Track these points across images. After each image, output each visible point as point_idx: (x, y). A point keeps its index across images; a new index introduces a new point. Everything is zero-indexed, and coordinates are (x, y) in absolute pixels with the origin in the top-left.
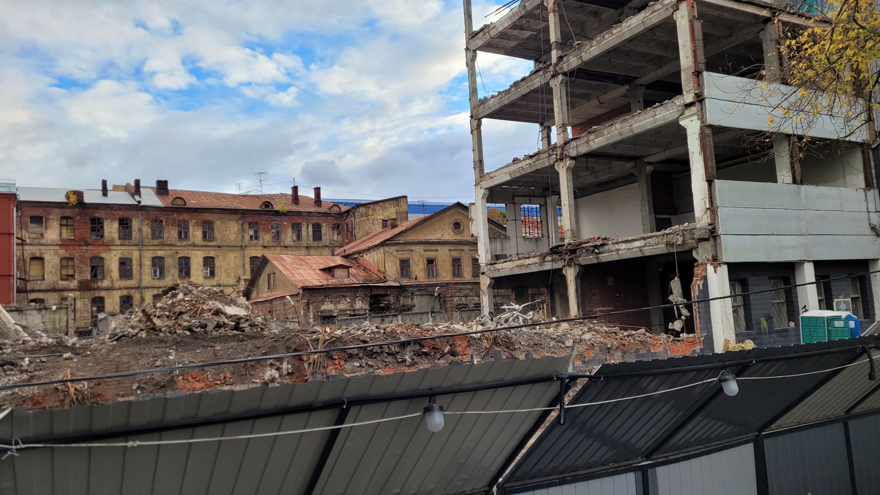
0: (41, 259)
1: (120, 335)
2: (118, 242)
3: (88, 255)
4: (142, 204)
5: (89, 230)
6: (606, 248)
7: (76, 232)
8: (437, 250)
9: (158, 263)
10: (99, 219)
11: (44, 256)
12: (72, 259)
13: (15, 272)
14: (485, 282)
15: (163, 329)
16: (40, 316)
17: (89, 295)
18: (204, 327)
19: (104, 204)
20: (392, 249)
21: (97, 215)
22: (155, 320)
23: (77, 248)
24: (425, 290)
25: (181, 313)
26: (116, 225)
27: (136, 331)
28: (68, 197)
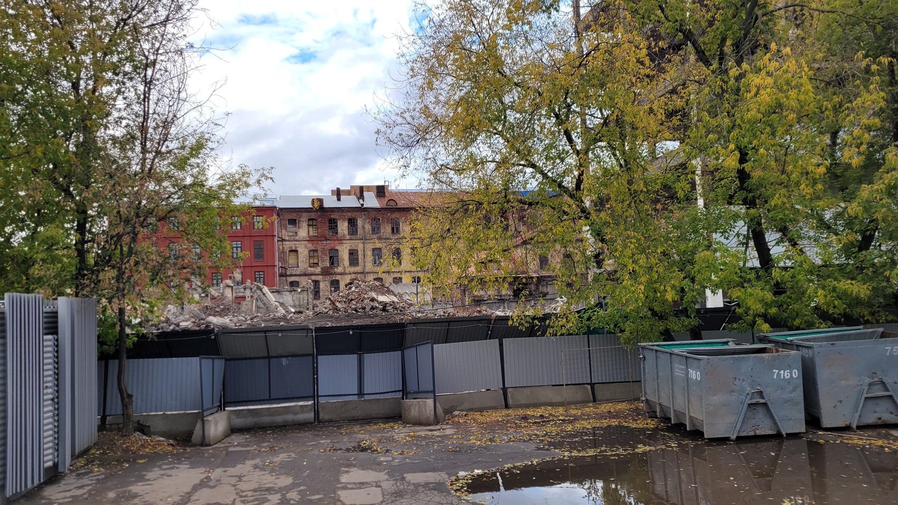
0: (296, 251)
2: (348, 237)
9: (377, 252)
12: (316, 251)
13: (277, 263)
17: (328, 278)
18: (364, 308)
21: (332, 217)
22: (337, 304)
25: (352, 300)
26: (346, 224)
28: (313, 204)
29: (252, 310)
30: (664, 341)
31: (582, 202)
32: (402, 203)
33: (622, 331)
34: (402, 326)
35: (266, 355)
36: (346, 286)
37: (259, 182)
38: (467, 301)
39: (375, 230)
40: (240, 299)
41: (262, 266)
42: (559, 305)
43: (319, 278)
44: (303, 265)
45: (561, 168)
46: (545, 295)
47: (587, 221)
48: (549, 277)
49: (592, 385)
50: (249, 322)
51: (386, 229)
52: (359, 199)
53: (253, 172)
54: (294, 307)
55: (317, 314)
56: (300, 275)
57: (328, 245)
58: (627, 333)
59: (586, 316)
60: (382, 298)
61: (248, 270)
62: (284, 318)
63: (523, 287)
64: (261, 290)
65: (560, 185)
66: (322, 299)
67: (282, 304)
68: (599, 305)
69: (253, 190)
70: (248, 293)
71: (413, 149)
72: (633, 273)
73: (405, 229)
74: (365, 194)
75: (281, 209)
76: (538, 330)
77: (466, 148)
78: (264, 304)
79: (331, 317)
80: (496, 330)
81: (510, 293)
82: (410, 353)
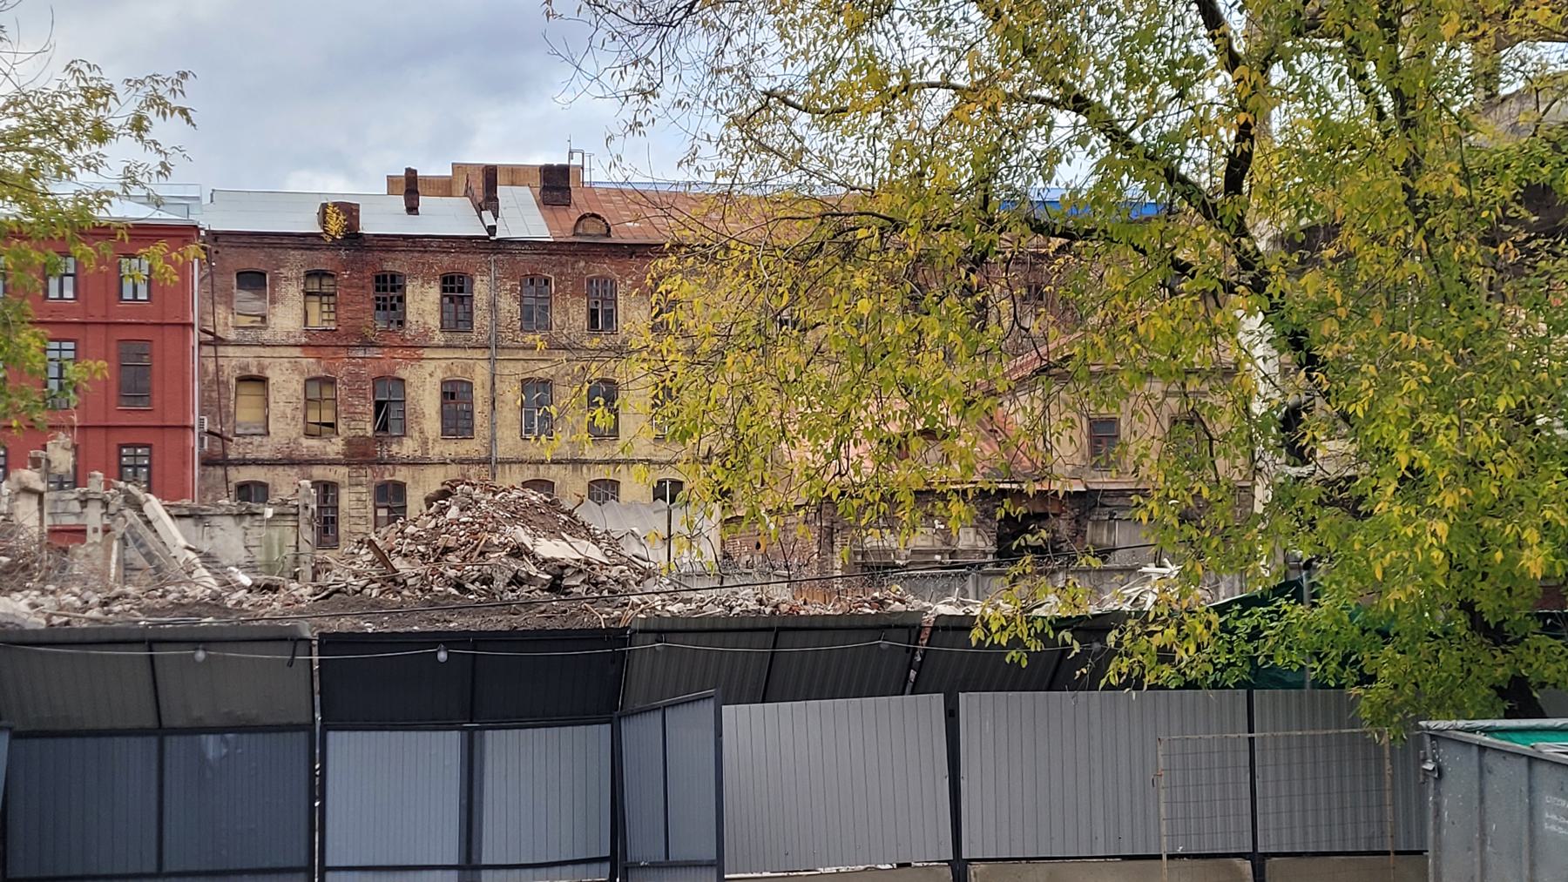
0: (262, 380)
1: (331, 588)
2: (439, 338)
3: (370, 371)
4: (499, 235)
5: (370, 306)
7: (341, 311)
9: (537, 390)
10: (393, 278)
11: (268, 373)
12: (331, 382)
13: (194, 420)
15: (410, 582)
16: (239, 532)
17: (369, 475)
18: (487, 580)
19: (406, 237)
21: (389, 267)
22: (398, 563)
23: (343, 353)
25: (447, 550)
26: (434, 292)
27: (362, 583)
28: (324, 221)
29: (105, 574)
30: (1507, 717)
31: (1242, 231)
32: (628, 230)
33: (1367, 679)
34: (616, 637)
35: (150, 722)
36: (429, 501)
37: (138, 125)
38: (839, 559)
39: (533, 317)
40: (66, 537)
41: (144, 429)
42: (1151, 587)
43: (339, 474)
44: (285, 429)
45: (1175, 117)
46: (1104, 553)
47: (1253, 300)
48: (1122, 493)
49: (1258, 860)
50: (95, 613)
51: (571, 316)
52: (480, 209)
53: (120, 89)
54: (250, 568)
55: (329, 595)
56: (272, 463)
57: (373, 361)
58: (1381, 689)
59: (1244, 626)
60: (548, 548)
61: (96, 438)
62: (215, 603)
63: (1024, 525)
64: (138, 507)
65: (1172, 176)
66: (346, 547)
67: (208, 559)
68: (1290, 589)
69: (122, 152)
70: (94, 517)
71: (674, 33)
72: (1413, 479)
73: (633, 317)
74: (503, 192)
75: (215, 236)
76: (1080, 660)
77: (855, 30)
78: (149, 556)
79: (376, 604)
80: (940, 664)
81: (987, 544)
82: (640, 733)
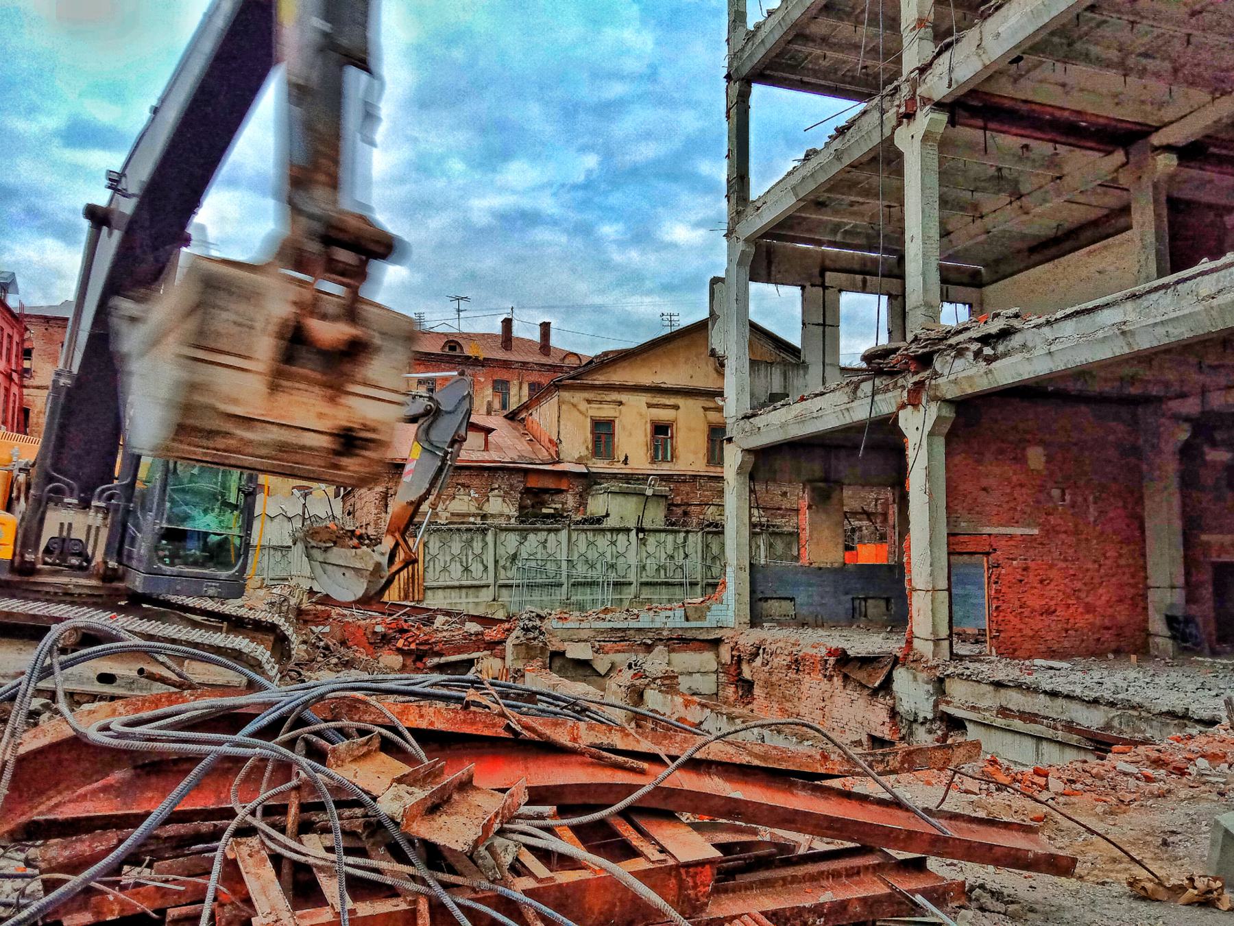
6: (1016, 340)
8: (676, 407)
14: (733, 457)
20: (578, 397)
24: (630, 483)
